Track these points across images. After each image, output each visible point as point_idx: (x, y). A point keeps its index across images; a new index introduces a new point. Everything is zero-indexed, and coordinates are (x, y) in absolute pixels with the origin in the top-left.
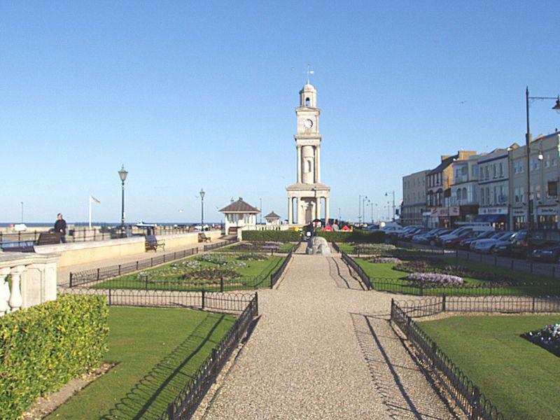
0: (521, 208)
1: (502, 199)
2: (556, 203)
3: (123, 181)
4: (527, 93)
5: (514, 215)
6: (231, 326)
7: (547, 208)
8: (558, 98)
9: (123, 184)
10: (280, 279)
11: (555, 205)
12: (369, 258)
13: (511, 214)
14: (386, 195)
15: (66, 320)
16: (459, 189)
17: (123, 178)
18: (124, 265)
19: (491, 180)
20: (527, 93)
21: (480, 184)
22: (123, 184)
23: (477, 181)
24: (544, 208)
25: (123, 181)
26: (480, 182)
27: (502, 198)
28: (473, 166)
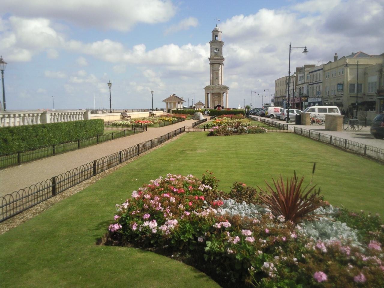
0: (327, 98)
1: (318, 93)
2: (342, 95)
3: (110, 88)
4: (290, 46)
5: (325, 102)
6: (342, 119)
7: (338, 98)
8: (305, 48)
9: (110, 89)
10: (301, 118)
11: (342, 96)
12: (221, 160)
13: (323, 102)
14: (264, 91)
15: (43, 225)
16: (300, 88)
17: (110, 86)
18: (171, 133)
19: (315, 82)
20: (290, 46)
21: (309, 85)
22: (110, 89)
23: (308, 83)
24: (337, 98)
25: (110, 88)
26: (310, 84)
27: (318, 93)
28: (300, 77)
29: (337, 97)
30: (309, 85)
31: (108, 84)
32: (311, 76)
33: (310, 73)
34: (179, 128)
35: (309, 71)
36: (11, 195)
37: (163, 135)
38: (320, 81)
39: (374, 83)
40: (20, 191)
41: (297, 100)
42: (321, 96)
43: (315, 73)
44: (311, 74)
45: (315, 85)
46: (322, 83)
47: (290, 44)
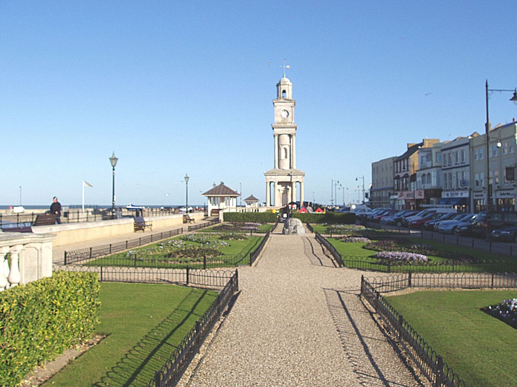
0: (481, 191)
1: (464, 183)
4: (487, 86)
7: (505, 192)
9: (114, 170)
11: (512, 189)
14: (357, 179)
16: (424, 175)
17: (114, 164)
20: (487, 86)
21: (443, 170)
22: (114, 170)
23: (441, 167)
25: (114, 167)
26: (443, 168)
27: (464, 183)
29: (501, 190)
30: (443, 170)
31: (110, 159)
32: (445, 155)
33: (442, 150)
34: (139, 237)
35: (441, 147)
36: (225, 272)
37: (114, 242)
38: (451, 165)
39: (136, 228)
40: (319, 261)
41: (419, 195)
42: (468, 187)
43: (454, 150)
44: (444, 152)
45: (454, 171)
46: (468, 168)
47: (487, 83)
